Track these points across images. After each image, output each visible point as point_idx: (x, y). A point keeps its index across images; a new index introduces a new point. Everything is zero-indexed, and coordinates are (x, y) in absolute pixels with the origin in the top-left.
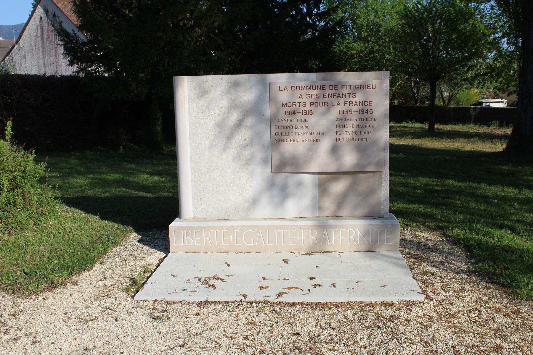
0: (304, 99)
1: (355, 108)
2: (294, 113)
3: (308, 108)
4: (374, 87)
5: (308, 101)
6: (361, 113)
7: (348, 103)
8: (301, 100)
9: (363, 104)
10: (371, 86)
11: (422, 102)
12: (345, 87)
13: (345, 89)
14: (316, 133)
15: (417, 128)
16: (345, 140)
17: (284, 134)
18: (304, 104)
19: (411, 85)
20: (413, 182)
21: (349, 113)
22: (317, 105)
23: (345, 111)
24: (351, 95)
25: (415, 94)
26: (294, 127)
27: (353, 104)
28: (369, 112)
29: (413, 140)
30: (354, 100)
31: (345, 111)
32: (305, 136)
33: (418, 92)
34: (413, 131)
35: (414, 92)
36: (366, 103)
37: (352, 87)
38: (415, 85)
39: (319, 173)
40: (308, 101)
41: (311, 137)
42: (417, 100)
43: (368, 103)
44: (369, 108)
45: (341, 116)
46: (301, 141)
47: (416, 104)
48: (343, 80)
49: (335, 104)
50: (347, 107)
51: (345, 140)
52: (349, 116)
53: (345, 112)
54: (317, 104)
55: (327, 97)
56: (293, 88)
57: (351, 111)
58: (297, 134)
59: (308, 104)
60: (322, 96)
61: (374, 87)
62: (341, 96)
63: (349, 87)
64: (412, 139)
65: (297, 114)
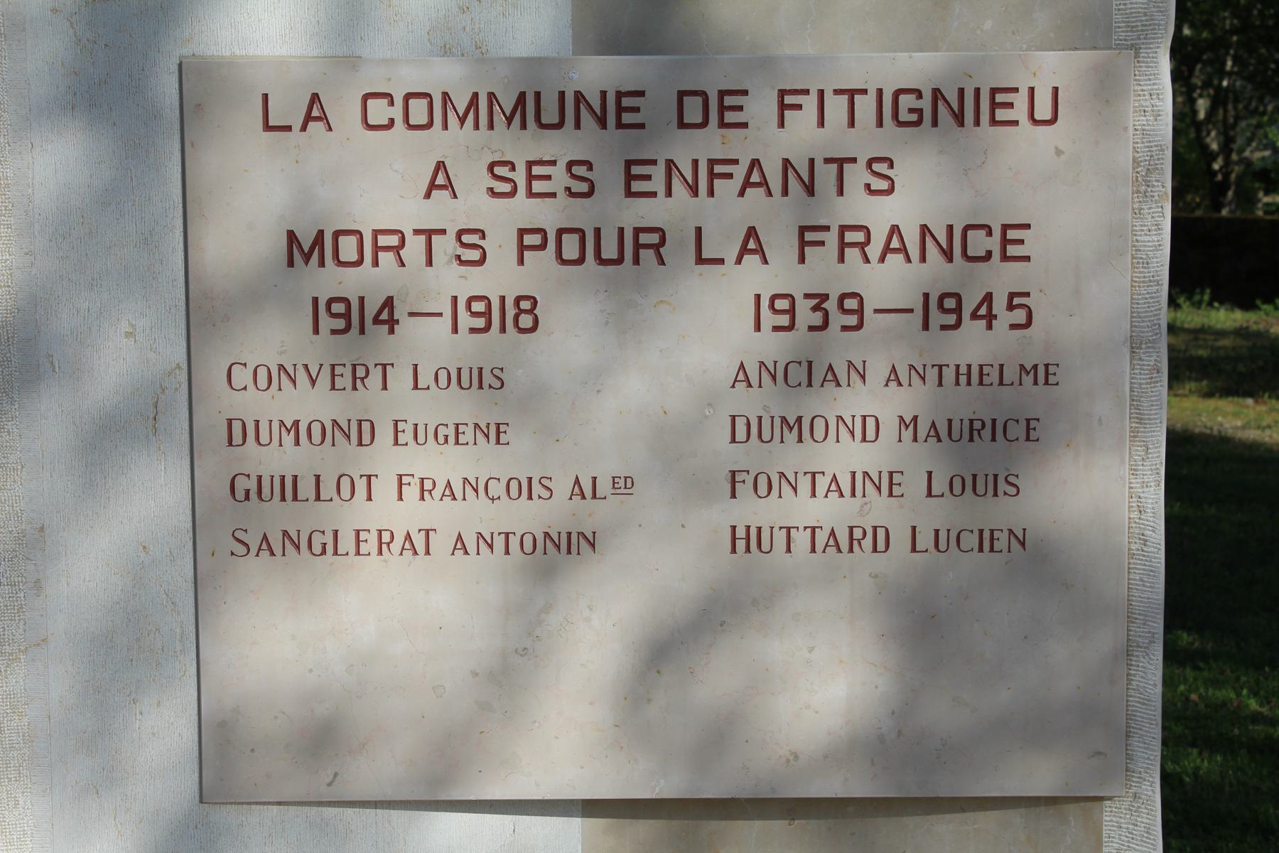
0: (473, 204)
1: (886, 282)
2: (387, 315)
3: (501, 277)
4: (1043, 112)
5: (504, 219)
6: (937, 318)
7: (832, 238)
8: (441, 212)
9: (953, 244)
10: (1021, 100)
11: (1246, 199)
12: (810, 103)
13: (803, 120)
14: (562, 487)
15: (1221, 334)
16: (801, 540)
17: (306, 489)
18: (471, 244)
19: (1195, 112)
20: (1253, 704)
21: (837, 319)
22: (571, 251)
23: (803, 307)
24: (857, 176)
25: (1212, 157)
26: (385, 433)
27: (874, 250)
28: (1004, 317)
29: (1211, 403)
30: (880, 215)
31: (803, 307)
32: (477, 504)
33: (1226, 148)
34: (1202, 353)
35: (1204, 148)
36: (979, 244)
37: (866, 106)
38: (1211, 113)
39: (590, 808)
40: (504, 219)
41: (528, 517)
42: (1223, 187)
43: (994, 243)
44: (1001, 279)
45: (772, 346)
46: (442, 543)
47: (1218, 207)
48: (788, 49)
49: (723, 244)
50: (822, 270)
51: (801, 540)
52: (839, 348)
53: (806, 315)
54: (571, 248)
55: (657, 184)
56: (379, 112)
57: (853, 307)
58: (411, 492)
59: (501, 246)
60: (609, 177)
61: (1043, 112)
62: (775, 183)
63: (836, 108)
64: (1209, 395)
65: (407, 326)
